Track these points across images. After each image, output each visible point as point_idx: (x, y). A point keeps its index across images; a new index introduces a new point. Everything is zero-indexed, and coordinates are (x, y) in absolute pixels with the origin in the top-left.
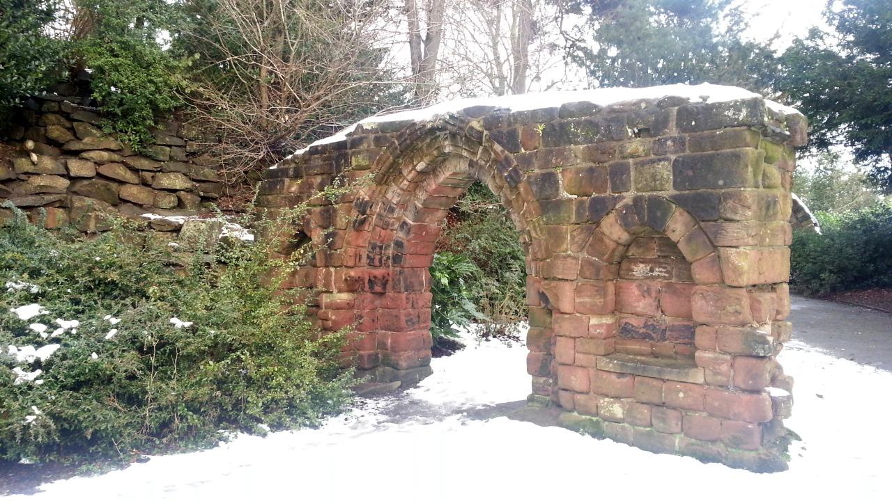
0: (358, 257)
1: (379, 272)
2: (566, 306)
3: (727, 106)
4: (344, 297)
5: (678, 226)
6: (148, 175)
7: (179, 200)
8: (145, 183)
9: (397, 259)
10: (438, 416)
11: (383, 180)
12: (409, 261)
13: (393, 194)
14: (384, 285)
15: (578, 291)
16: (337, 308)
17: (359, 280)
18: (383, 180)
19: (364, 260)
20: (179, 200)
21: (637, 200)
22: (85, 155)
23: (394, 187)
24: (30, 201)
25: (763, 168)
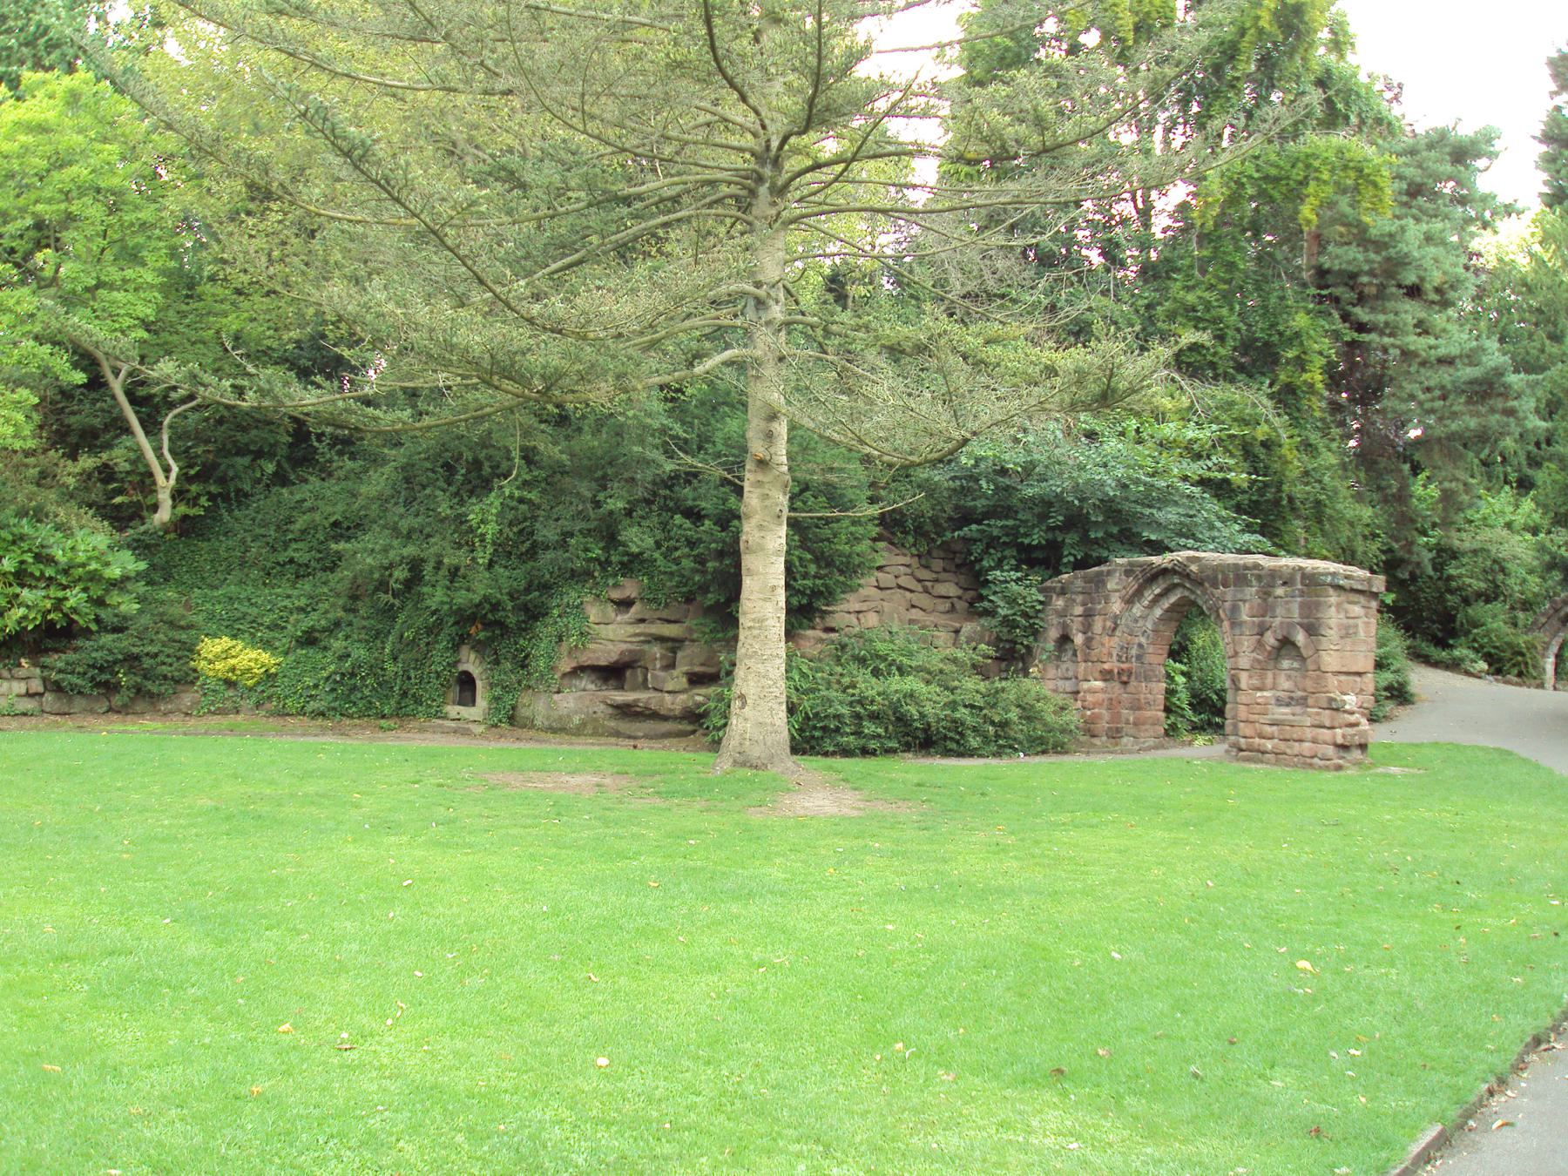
0: (1110, 655)
1: (1125, 666)
2: (1243, 685)
3: (1327, 574)
4: (1099, 684)
5: (1300, 638)
6: (929, 584)
7: (953, 604)
8: (926, 591)
9: (1139, 657)
10: (863, 17)
11: (1129, 601)
12: (1148, 659)
13: (1137, 610)
14: (1129, 677)
15: (1250, 677)
16: (1093, 691)
17: (1110, 672)
18: (1129, 601)
19: (1115, 658)
20: (953, 604)
21: (1282, 623)
22: (887, 569)
23: (1138, 605)
24: (857, 607)
25: (980, 659)
